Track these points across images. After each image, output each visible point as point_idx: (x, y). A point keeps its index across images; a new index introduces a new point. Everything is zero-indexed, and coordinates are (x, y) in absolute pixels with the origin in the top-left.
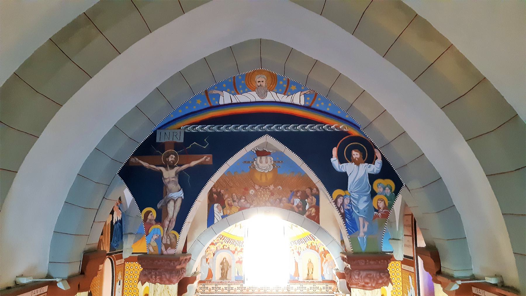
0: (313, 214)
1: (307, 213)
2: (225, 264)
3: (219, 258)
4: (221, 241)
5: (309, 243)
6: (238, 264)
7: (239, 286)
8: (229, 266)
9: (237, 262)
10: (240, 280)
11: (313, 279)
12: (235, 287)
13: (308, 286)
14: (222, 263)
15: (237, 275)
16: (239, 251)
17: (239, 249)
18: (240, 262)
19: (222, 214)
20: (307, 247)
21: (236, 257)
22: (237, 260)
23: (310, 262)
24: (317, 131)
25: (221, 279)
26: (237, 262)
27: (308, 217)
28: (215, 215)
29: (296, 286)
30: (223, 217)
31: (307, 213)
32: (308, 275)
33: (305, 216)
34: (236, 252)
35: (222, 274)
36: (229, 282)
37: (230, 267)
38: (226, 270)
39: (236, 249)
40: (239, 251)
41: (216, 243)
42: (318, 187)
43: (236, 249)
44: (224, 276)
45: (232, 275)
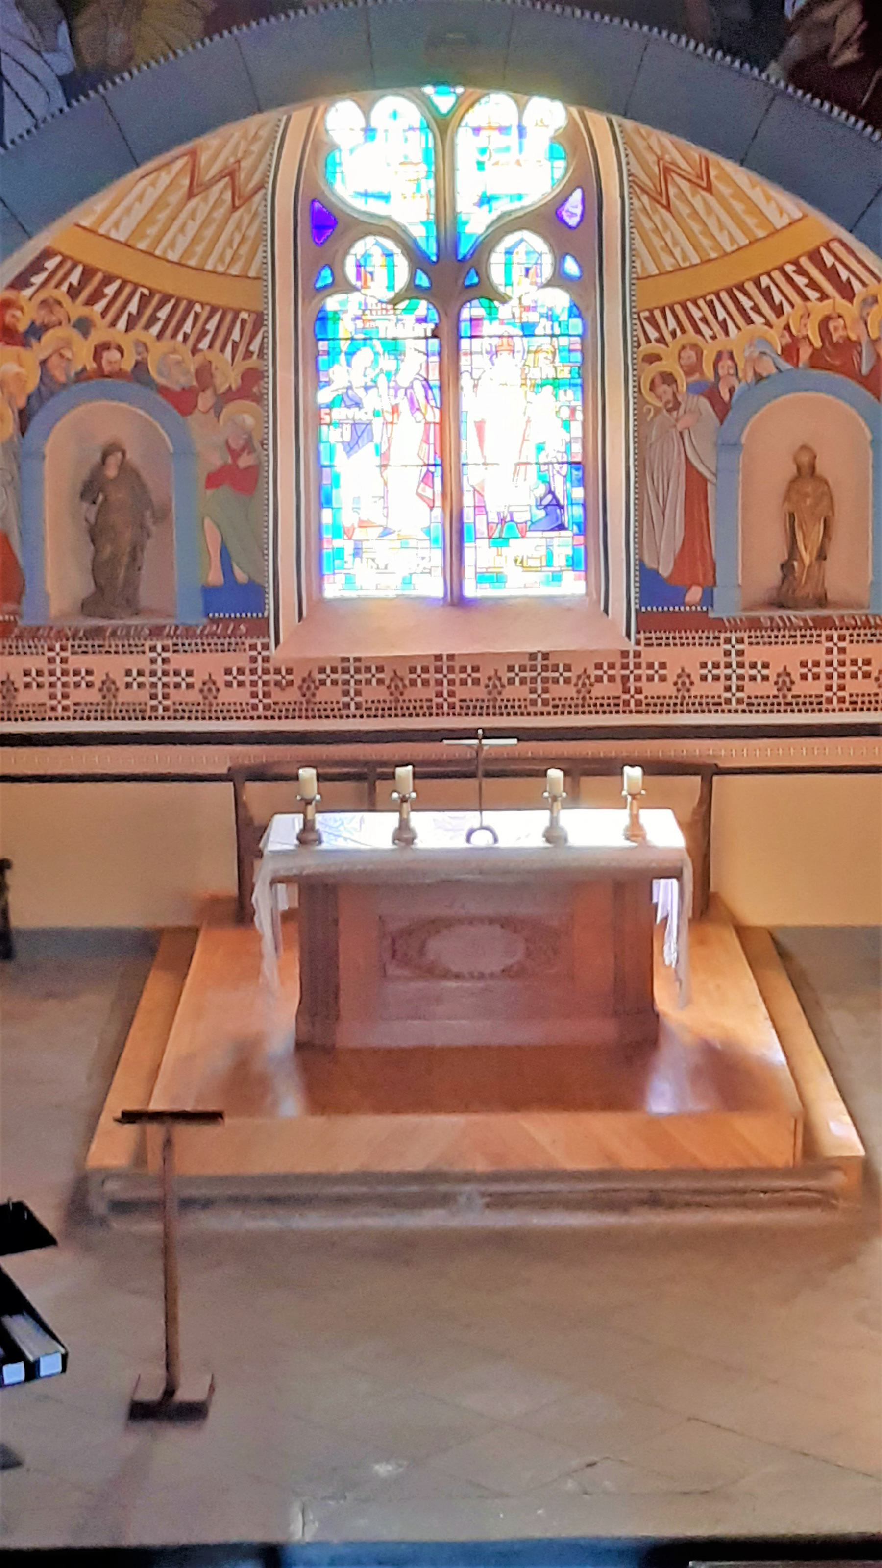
0: (850, 55)
1: (795, 47)
2: (119, 495)
3: (65, 447)
4: (77, 309)
5: (805, 318)
6: (225, 492)
7: (240, 660)
8: (148, 511)
9: (213, 480)
10: (239, 606)
11: (822, 601)
12: (206, 664)
13: (785, 656)
14: (91, 489)
15: (215, 577)
16: (229, 396)
17: (228, 375)
18: (241, 477)
19: (64, 63)
20: (790, 352)
21: (209, 437)
22: (217, 460)
23: (807, 471)
24: (435, 85)
25: (87, 607)
26: (213, 480)
27: (801, 75)
28: (10, 71)
29: (684, 657)
30: (73, 86)
31: (795, 47)
32: (786, 567)
33: (775, 70)
34: (205, 400)
35: (99, 570)
36: (156, 632)
37: (162, 515)
38: (128, 536)
39: (204, 374)
40: (229, 396)
41: (36, 331)
42: (37, 253)
43: (204, 374)
44: (111, 592)
45: (180, 566)
